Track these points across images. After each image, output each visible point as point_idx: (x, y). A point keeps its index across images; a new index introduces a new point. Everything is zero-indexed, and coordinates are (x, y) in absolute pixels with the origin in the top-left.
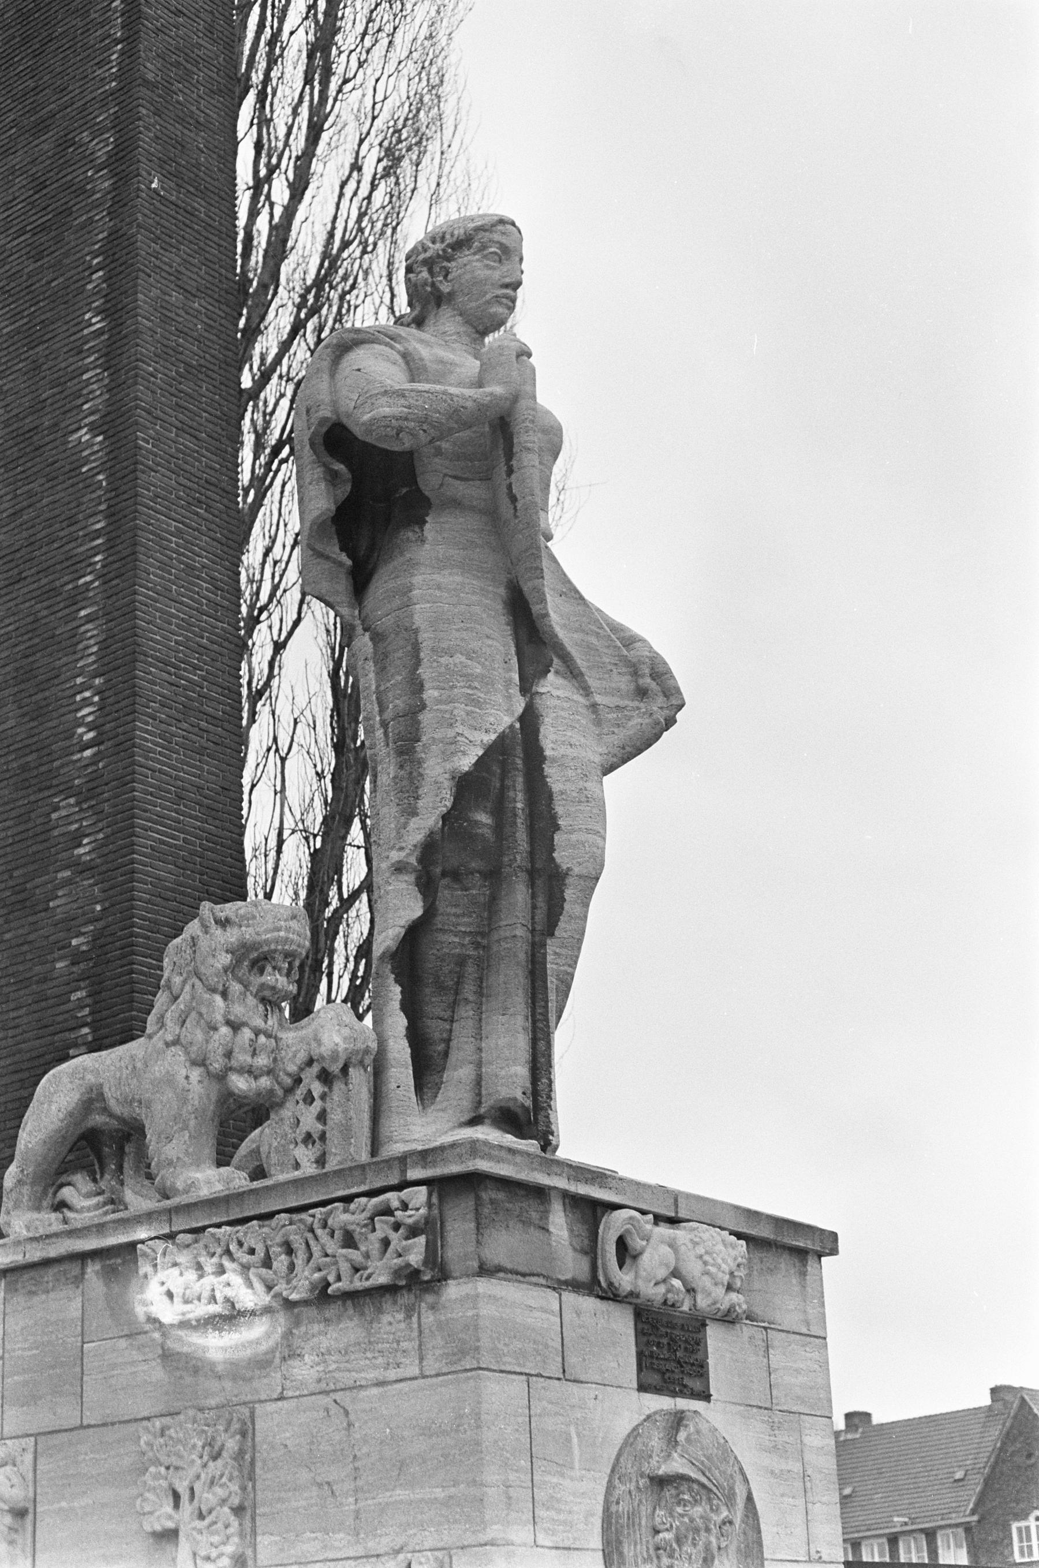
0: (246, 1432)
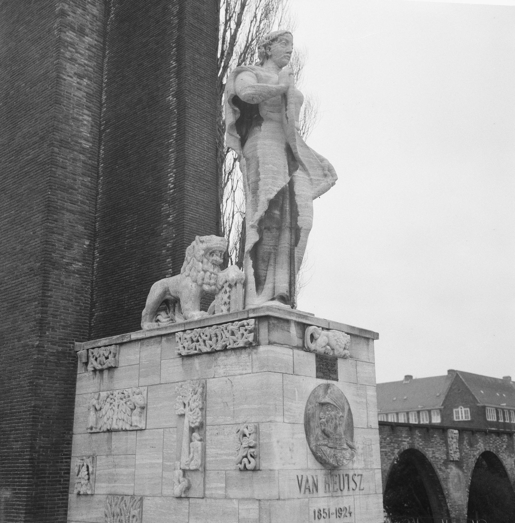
0: (204, 387)
